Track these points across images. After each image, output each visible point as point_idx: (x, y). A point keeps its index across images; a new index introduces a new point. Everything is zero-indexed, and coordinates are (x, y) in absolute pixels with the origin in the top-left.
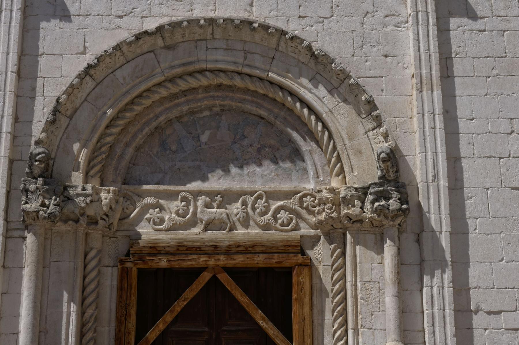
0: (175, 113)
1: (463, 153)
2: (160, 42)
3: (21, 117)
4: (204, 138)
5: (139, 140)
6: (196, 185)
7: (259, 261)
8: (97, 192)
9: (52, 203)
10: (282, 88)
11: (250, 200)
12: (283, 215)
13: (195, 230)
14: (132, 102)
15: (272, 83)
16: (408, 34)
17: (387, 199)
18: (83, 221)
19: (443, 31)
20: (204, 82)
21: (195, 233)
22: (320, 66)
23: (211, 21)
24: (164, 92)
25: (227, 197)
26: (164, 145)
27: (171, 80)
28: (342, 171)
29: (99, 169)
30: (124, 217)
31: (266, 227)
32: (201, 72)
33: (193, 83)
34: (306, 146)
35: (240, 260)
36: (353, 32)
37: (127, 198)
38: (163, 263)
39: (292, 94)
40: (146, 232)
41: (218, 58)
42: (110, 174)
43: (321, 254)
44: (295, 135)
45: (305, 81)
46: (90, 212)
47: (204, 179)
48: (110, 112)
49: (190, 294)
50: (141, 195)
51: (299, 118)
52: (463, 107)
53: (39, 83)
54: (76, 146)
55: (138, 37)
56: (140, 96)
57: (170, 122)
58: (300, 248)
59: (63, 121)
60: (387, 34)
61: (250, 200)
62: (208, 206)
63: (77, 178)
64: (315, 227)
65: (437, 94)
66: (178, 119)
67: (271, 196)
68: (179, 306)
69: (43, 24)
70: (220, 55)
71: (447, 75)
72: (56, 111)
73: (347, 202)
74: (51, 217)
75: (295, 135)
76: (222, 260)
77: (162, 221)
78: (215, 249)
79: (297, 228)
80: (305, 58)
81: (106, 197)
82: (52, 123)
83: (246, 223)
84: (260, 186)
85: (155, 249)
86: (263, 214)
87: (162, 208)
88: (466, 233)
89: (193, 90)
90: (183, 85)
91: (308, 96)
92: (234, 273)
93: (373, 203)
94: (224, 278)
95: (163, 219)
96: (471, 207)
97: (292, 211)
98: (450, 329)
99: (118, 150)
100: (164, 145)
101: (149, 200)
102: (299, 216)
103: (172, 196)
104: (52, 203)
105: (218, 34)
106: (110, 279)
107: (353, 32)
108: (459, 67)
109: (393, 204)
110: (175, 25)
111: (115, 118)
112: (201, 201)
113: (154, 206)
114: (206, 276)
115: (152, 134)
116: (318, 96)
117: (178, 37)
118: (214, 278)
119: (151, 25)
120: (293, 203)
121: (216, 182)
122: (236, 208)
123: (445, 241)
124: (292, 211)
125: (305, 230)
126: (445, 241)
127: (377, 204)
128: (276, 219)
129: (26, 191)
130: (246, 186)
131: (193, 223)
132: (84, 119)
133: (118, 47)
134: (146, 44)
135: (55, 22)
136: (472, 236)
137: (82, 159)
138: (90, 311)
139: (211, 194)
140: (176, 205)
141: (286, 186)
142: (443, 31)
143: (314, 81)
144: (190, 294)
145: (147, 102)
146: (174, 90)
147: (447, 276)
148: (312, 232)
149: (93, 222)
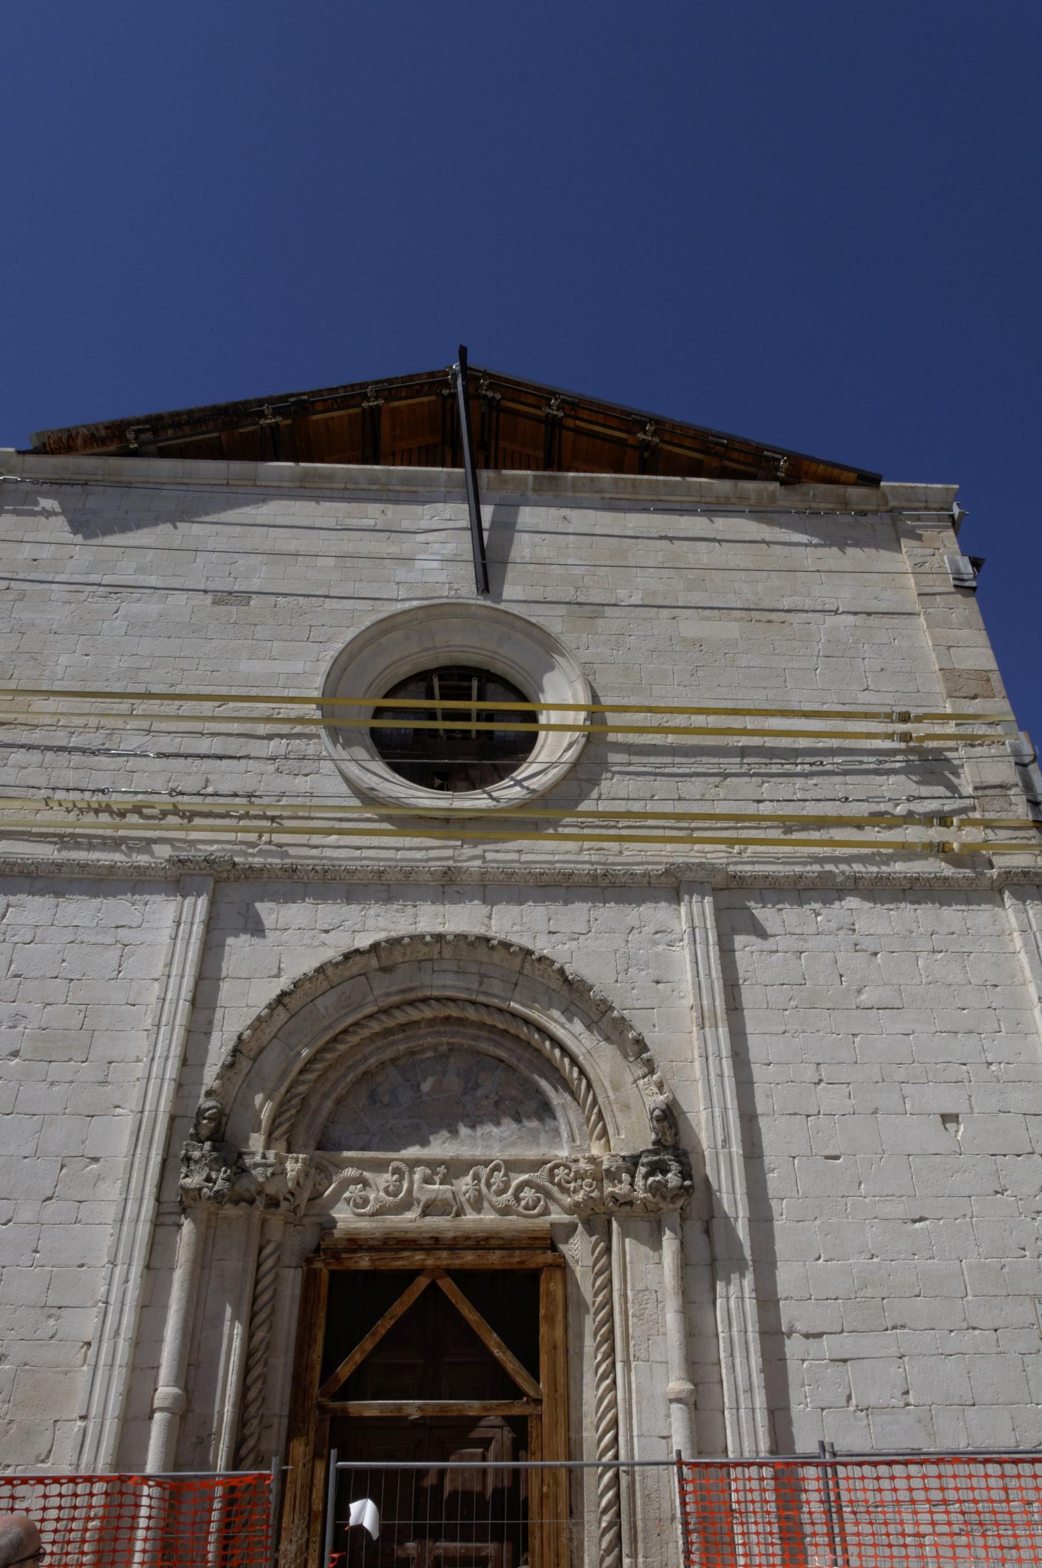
0: (388, 1054)
1: (760, 1110)
2: (374, 963)
3: (190, 1061)
4: (426, 1087)
5: (340, 1090)
6: (413, 1152)
7: (495, 1259)
8: (281, 1161)
9: (221, 1176)
10: (527, 1021)
11: (484, 1172)
12: (528, 1194)
13: (409, 1215)
14: (335, 1040)
15: (514, 1015)
16: (683, 955)
17: (665, 1172)
18: (260, 1203)
19: (727, 952)
20: (428, 1013)
21: (409, 1220)
22: (574, 994)
23: (439, 938)
24: (376, 1027)
25: (454, 1169)
26: (373, 1097)
27: (386, 1011)
28: (604, 1133)
29: (284, 1133)
30: (316, 1196)
31: (505, 1211)
32: (425, 1000)
33: (414, 1014)
34: (558, 1099)
35: (469, 1259)
36: (616, 951)
37: (320, 1170)
38: (364, 1262)
39: (541, 1030)
40: (345, 1217)
41: (445, 983)
42: (300, 1138)
43: (578, 1249)
44: (544, 1084)
45: (556, 1013)
46: (271, 1190)
47: (424, 1143)
48: (305, 1052)
49: (399, 1308)
50: (340, 1166)
51: (549, 1061)
52: (756, 1047)
53: (219, 1014)
54: (259, 1098)
55: (347, 957)
56: (345, 1031)
57: (382, 1065)
58: (549, 1242)
59: (244, 1065)
60: (657, 955)
61: (484, 1172)
62: (428, 1180)
63: (256, 1142)
64: (569, 1211)
65: (723, 1031)
66: (394, 1061)
67: (512, 1166)
68: (384, 1326)
69: (230, 941)
70: (449, 980)
71: (734, 1007)
72: (236, 1051)
73: (612, 1176)
74: (218, 1197)
75: (544, 1084)
76: (444, 1259)
77: (366, 1202)
78: (435, 1243)
79: (546, 1212)
80: (556, 983)
81: (293, 1167)
82: (230, 1067)
83: (477, 1205)
84: (497, 1153)
85: (355, 1243)
86: (501, 1192)
87: (366, 1184)
88: (769, 1220)
89: (413, 1024)
90: (401, 1018)
91: (560, 1033)
92: (462, 1276)
93: (646, 1177)
94: (447, 1285)
95: (373, 1198)
96: (774, 1181)
97: (539, 1189)
98: (756, 1362)
99: (313, 1103)
100: (373, 1097)
101: (350, 1172)
102: (548, 1195)
103: (380, 1166)
104: (221, 1176)
105: (448, 953)
106: (292, 1283)
107: (616, 951)
108: (748, 997)
109: (672, 1179)
110: (394, 942)
111: (312, 1061)
112: (419, 1173)
113: (356, 1181)
114: (422, 1283)
115: (358, 1081)
116: (574, 1033)
117: (397, 957)
118: (433, 1287)
119: (364, 942)
120: (540, 1176)
121: (441, 1148)
122: (465, 1184)
123: (742, 1231)
124: (539, 1189)
125: (557, 1216)
126: (742, 1231)
127: (651, 1179)
128: (518, 1200)
129: (188, 1159)
130: (478, 1152)
131: (406, 1205)
132: (271, 1062)
133: (321, 970)
134: (356, 966)
135: (244, 938)
136: (777, 1224)
137: (265, 1115)
138: (260, 1334)
139: (432, 1164)
140: (385, 1179)
141: (532, 1153)
142: (727, 952)
143: (568, 1012)
144: (399, 1308)
145: (354, 1040)
146: (390, 1023)
147: (748, 1282)
148: (566, 1218)
149: (273, 1203)
